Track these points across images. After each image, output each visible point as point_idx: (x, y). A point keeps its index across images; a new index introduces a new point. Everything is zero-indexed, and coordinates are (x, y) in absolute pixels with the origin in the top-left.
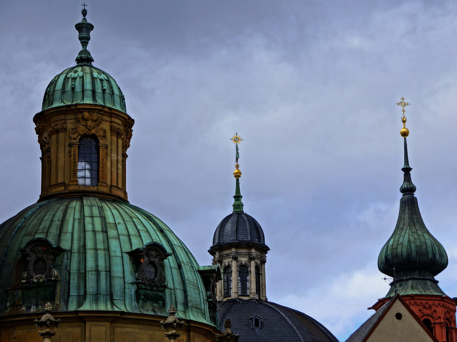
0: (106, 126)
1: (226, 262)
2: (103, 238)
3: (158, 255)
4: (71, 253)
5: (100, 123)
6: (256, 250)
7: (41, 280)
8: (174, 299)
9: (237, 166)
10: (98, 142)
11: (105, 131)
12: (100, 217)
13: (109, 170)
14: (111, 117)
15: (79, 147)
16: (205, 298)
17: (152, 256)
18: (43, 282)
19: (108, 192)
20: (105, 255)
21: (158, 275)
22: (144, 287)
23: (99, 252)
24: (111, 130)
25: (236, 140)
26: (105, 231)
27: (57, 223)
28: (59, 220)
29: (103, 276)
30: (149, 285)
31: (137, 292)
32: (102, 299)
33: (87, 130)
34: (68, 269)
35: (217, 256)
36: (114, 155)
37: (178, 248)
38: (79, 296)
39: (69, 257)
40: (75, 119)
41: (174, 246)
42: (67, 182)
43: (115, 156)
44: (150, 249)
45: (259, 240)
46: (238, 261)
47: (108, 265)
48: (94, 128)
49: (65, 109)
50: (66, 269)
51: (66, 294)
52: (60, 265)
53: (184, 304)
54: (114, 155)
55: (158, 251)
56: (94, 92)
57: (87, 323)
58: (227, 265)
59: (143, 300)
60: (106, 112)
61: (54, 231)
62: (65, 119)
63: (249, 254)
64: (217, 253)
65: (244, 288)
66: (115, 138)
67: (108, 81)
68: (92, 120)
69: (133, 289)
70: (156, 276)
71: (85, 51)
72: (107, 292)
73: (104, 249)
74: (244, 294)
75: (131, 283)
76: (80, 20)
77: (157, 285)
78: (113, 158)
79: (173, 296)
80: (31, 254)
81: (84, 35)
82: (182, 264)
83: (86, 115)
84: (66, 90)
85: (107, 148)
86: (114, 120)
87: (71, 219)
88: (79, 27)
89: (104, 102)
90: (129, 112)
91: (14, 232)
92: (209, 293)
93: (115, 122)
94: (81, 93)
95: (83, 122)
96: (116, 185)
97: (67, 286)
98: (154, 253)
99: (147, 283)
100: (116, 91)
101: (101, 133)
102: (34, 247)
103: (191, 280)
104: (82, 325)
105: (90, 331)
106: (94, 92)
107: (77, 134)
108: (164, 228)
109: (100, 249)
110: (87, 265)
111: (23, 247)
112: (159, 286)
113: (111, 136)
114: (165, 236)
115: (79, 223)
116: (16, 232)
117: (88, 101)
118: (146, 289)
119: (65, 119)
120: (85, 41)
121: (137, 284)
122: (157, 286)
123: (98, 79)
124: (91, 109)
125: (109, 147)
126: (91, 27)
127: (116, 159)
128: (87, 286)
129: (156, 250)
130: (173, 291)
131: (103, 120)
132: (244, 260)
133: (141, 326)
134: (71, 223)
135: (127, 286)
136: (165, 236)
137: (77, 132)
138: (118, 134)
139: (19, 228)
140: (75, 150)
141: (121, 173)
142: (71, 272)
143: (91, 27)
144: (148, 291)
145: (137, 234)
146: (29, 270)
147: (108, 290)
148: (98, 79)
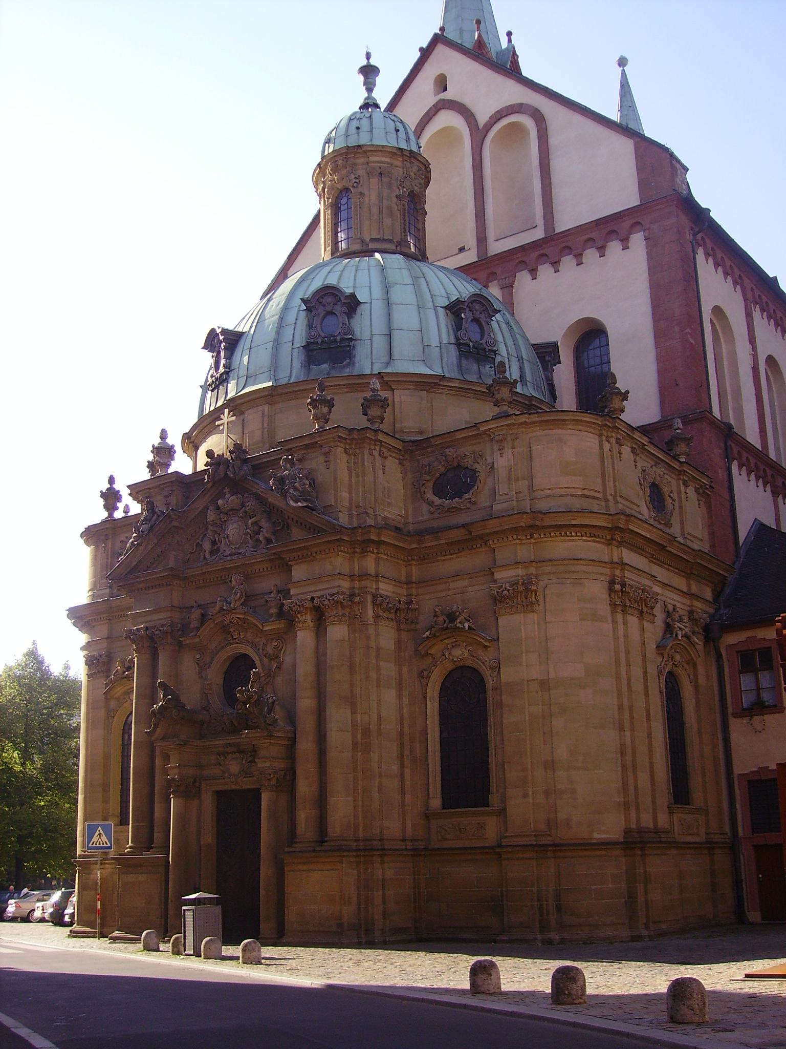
21: (486, 336)
76: (365, 62)
95: (357, 176)
98: (477, 307)
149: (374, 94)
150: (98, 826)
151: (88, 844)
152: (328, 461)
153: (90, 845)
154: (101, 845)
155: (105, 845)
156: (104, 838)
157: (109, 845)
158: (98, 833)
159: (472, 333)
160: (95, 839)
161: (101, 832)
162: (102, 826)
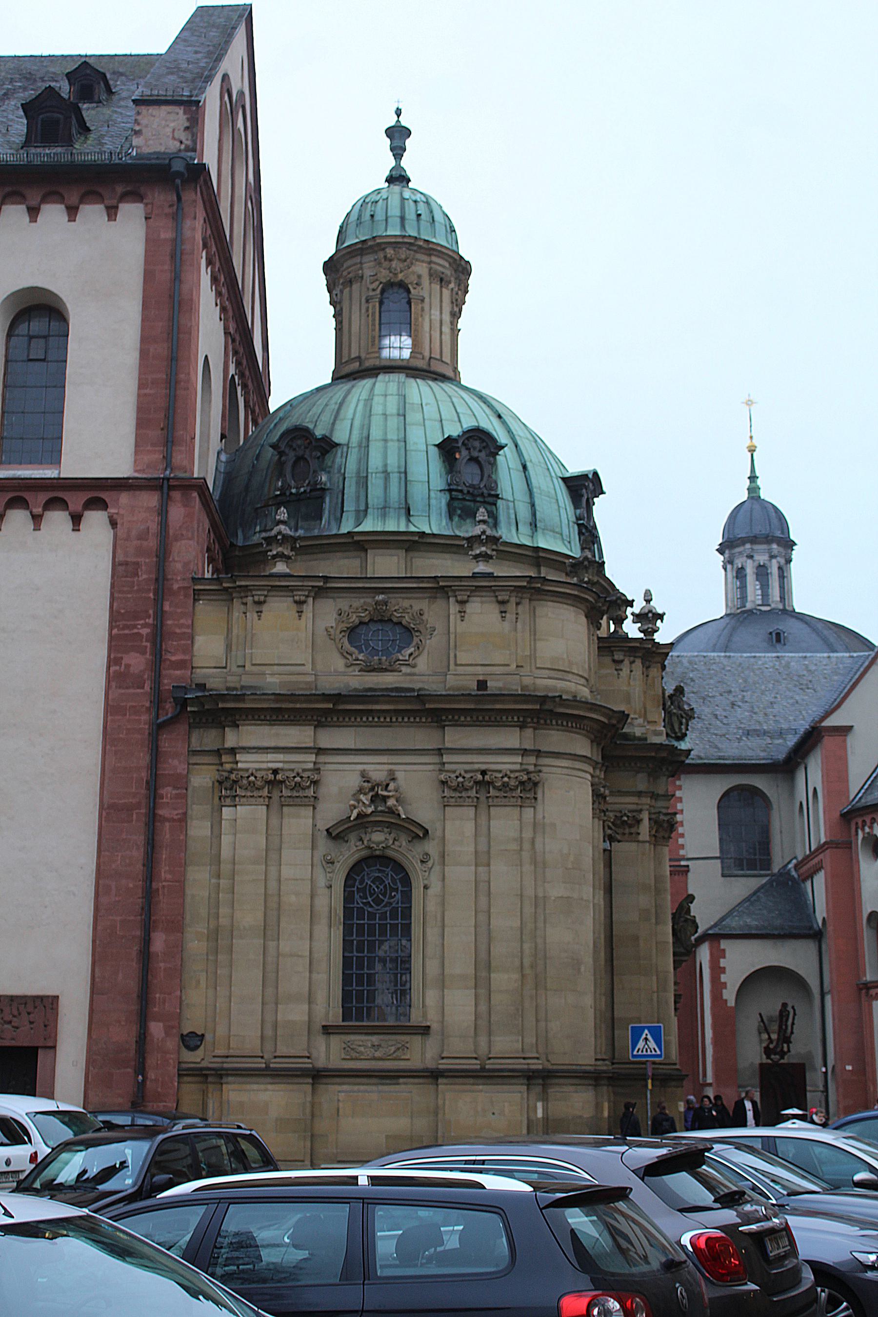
0: (421, 269)
1: (738, 563)
2: (398, 424)
3: (484, 448)
4: (348, 448)
5: (412, 264)
6: (778, 545)
7: (302, 490)
8: (513, 516)
9: (751, 437)
10: (409, 291)
11: (419, 277)
12: (399, 395)
13: (428, 335)
14: (430, 255)
15: (381, 303)
16: (574, 519)
17: (475, 448)
18: (305, 491)
19: (425, 367)
20: (399, 449)
21: (485, 478)
22: (460, 497)
23: (390, 444)
24: (431, 275)
25: (749, 403)
26: (402, 415)
27: (333, 406)
28: (336, 403)
29: (394, 479)
30: (468, 492)
31: (449, 505)
32: (392, 514)
33: (391, 275)
34: (343, 471)
35: (727, 555)
36: (436, 313)
37: (526, 441)
38: (357, 511)
39: (345, 455)
40: (375, 260)
41: (517, 437)
42: (363, 356)
43: (438, 313)
44: (471, 437)
45: (783, 533)
46: (754, 561)
47: (403, 463)
48: (401, 271)
49: (360, 246)
50: (339, 471)
51: (339, 510)
52: (331, 467)
53: (531, 524)
54: (436, 313)
55: (483, 441)
56: (403, 219)
57: (369, 551)
58: (740, 566)
59: (460, 516)
60: (420, 247)
61: (327, 418)
62: (361, 263)
63: (770, 551)
64: (727, 552)
65: (765, 595)
66: (436, 287)
67: (427, 203)
68: (400, 260)
69: (444, 499)
70: (482, 480)
71: (397, 167)
72: (400, 504)
73: (398, 440)
74: (765, 602)
75: (441, 491)
76: (392, 121)
77: (483, 493)
78: (433, 317)
79: (512, 511)
80: (287, 451)
81: (397, 143)
82: (528, 464)
83: (390, 252)
84: (363, 220)
85: (423, 301)
86: (434, 259)
87: (355, 401)
88: (391, 132)
89: (419, 233)
90: (465, 252)
91: (272, 425)
92: (578, 511)
93: (435, 263)
94: (384, 222)
95: (386, 264)
96: (438, 357)
97: (340, 496)
98: (477, 444)
99: (465, 490)
100: (438, 217)
101: (413, 279)
102: (292, 440)
103: (544, 487)
104: (363, 554)
105: (374, 563)
106: (403, 219)
107: (377, 283)
108: (504, 412)
109: (392, 440)
110: (370, 464)
111: (275, 440)
112: (486, 495)
113: (430, 283)
114: (504, 423)
115: (365, 405)
116: (275, 425)
117: (394, 230)
118: (464, 499)
119: (361, 263)
120: (398, 151)
121: (450, 491)
122: (482, 495)
123: (410, 201)
124: (397, 244)
125: (427, 300)
126: (408, 133)
127: (438, 318)
128: (369, 496)
129: (480, 439)
130: (511, 505)
131: (417, 260)
132: (762, 558)
133: (455, 556)
134: (353, 406)
135: (432, 494)
136: (504, 423)
137: (377, 280)
138: (442, 281)
139: (281, 419)
140: (374, 306)
141: (449, 342)
142: (346, 475)
143: (408, 133)
144: (468, 503)
145: (456, 419)
146: (285, 476)
147: (403, 501)
148: (410, 201)
149: (403, 163)
150: (643, 1029)
151: (633, 1050)
152: (505, 612)
153: (635, 1053)
154: (649, 1053)
155: (653, 1053)
156: (652, 1044)
157: (659, 1052)
158: (644, 1036)
159: (469, 475)
160: (641, 1044)
161: (649, 1037)
162: (648, 1028)
